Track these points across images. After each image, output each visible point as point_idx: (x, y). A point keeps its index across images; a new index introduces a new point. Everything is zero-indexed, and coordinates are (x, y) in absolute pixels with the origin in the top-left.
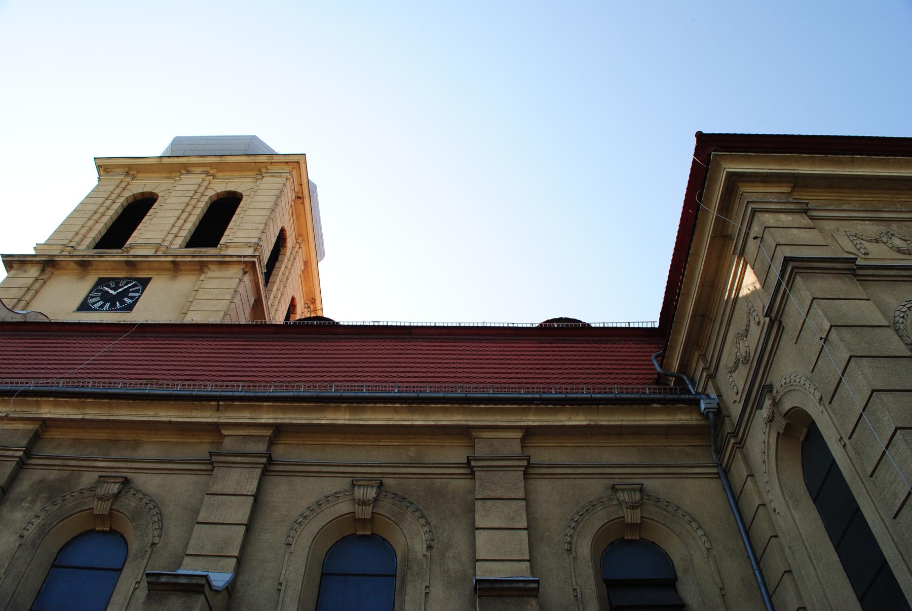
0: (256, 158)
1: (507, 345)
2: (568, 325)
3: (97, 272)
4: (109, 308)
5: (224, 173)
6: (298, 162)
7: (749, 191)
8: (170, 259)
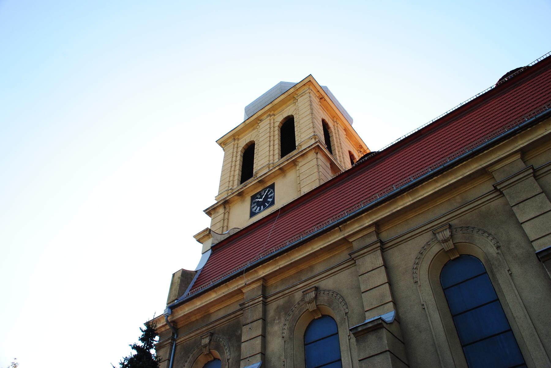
0: (288, 93)
2: (514, 74)
6: (310, 81)
8: (277, 168)
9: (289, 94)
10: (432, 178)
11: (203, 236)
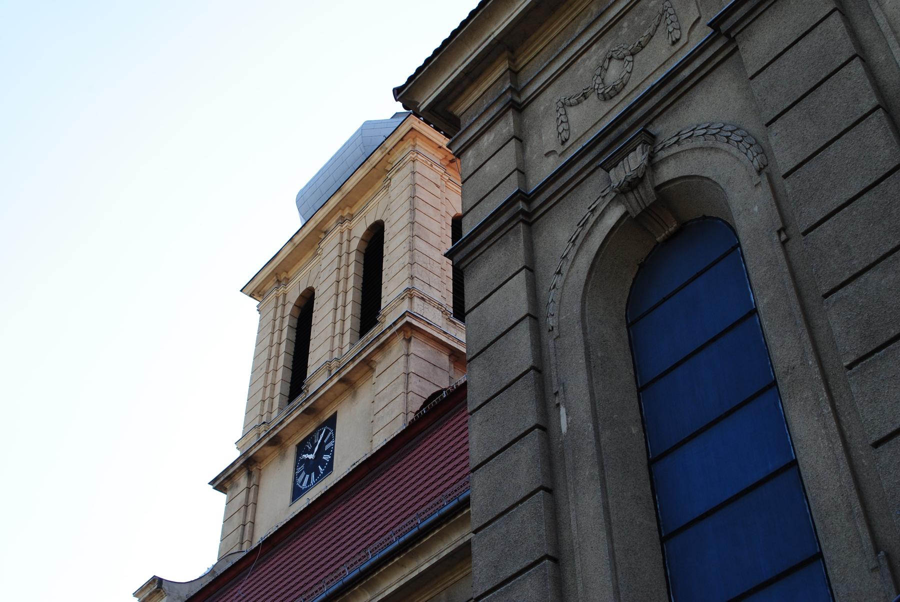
2: (438, 399)
4: (315, 480)
5: (357, 204)
6: (412, 129)
7: (421, 145)
8: (336, 380)
10: (392, 559)
11: (150, 594)
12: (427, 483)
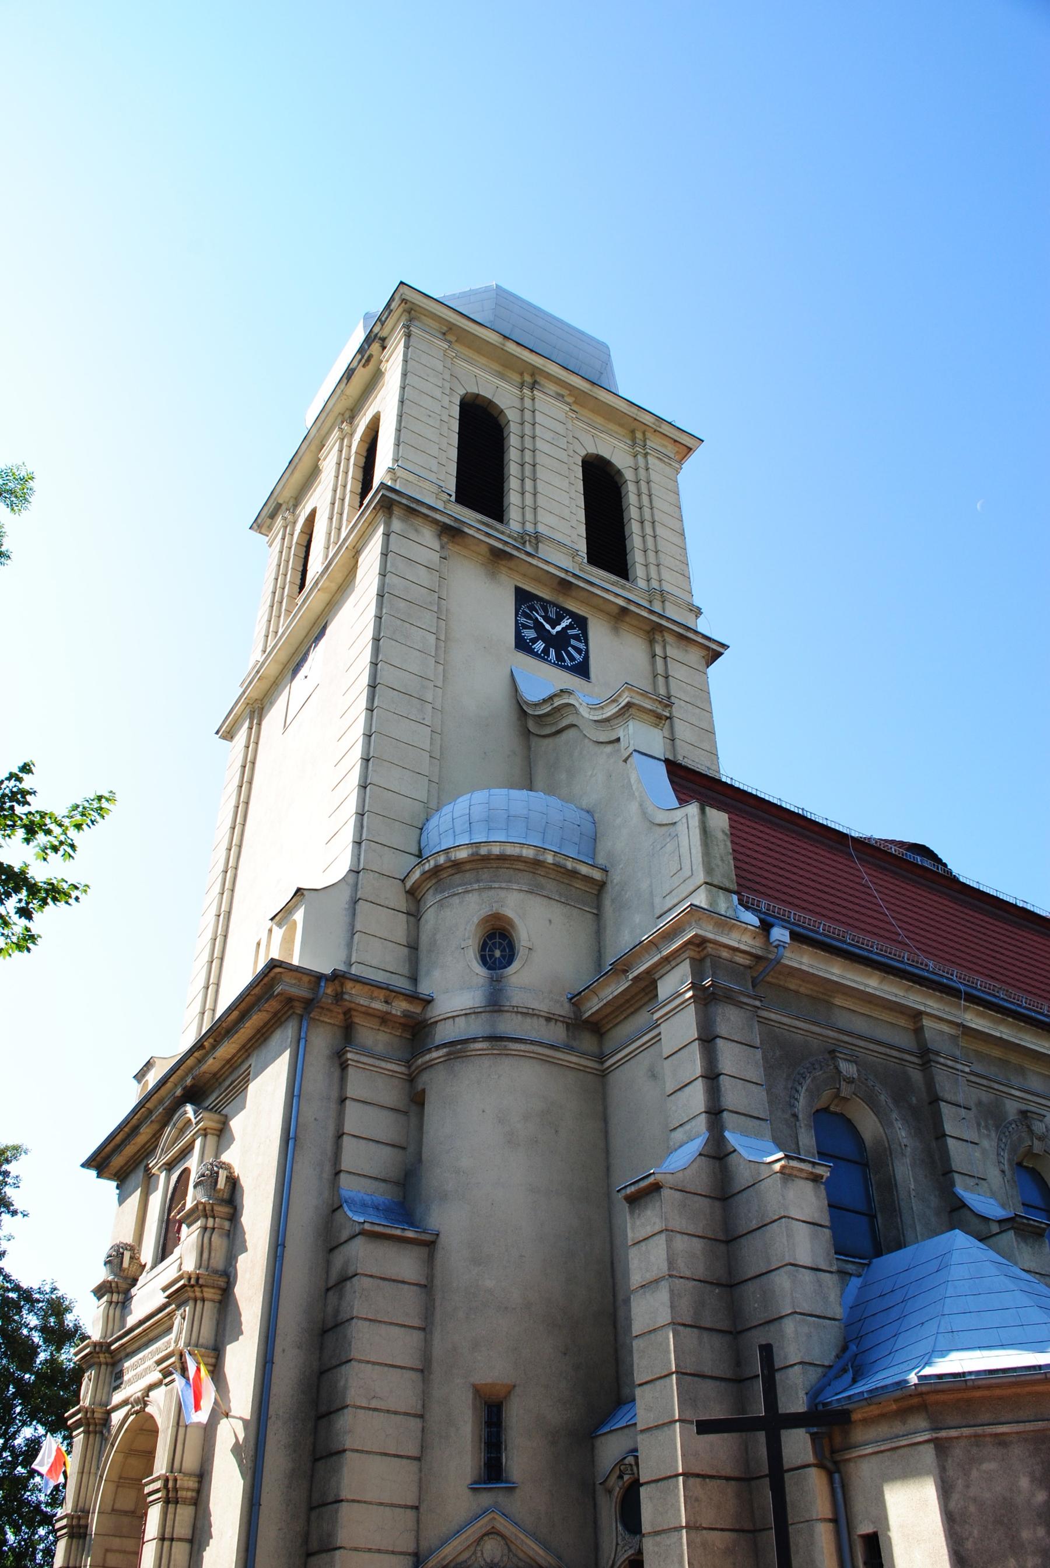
0: (639, 413)
1: (835, 858)
3: (509, 572)
9: (638, 418)
11: (651, 710)
12: (1031, 975)
